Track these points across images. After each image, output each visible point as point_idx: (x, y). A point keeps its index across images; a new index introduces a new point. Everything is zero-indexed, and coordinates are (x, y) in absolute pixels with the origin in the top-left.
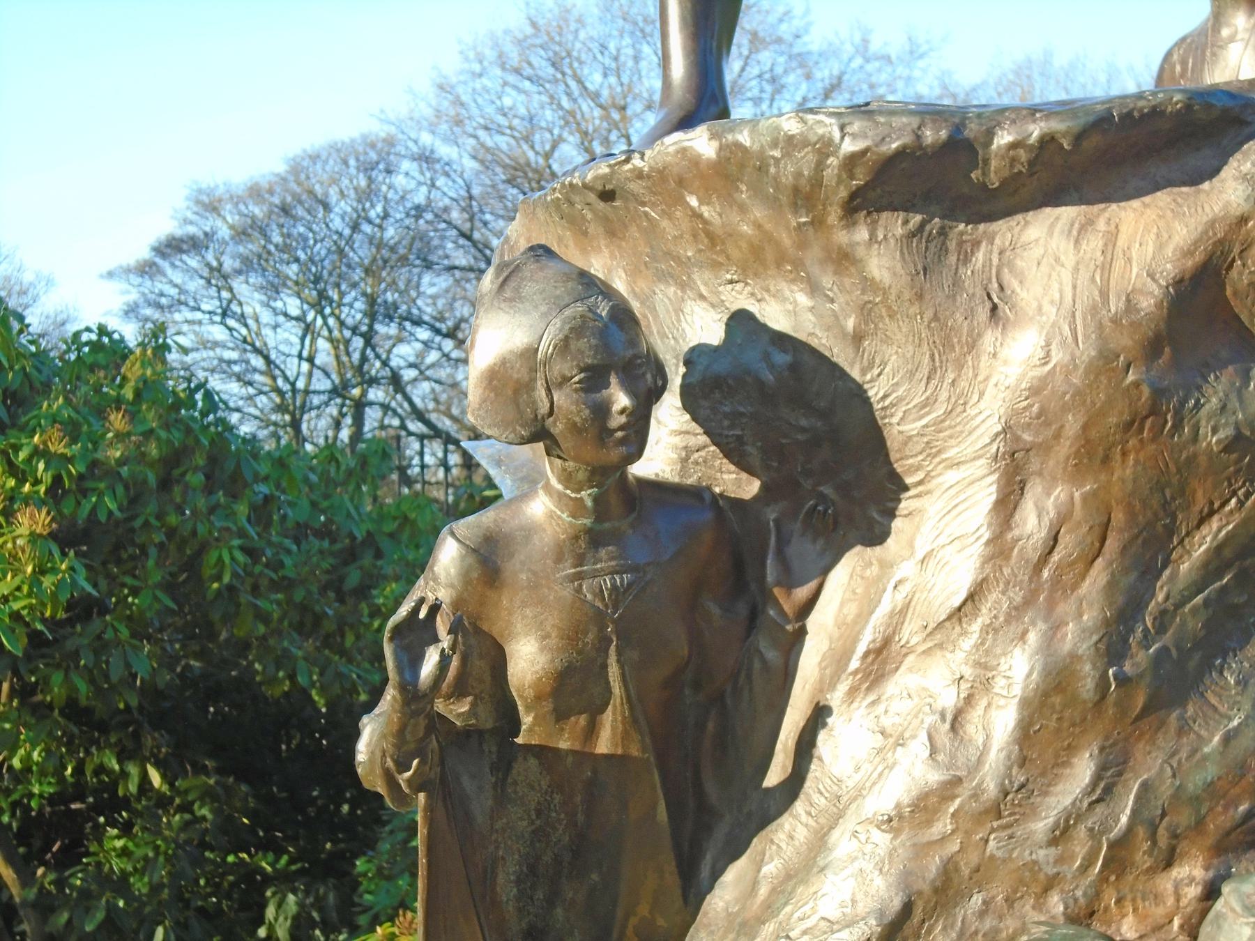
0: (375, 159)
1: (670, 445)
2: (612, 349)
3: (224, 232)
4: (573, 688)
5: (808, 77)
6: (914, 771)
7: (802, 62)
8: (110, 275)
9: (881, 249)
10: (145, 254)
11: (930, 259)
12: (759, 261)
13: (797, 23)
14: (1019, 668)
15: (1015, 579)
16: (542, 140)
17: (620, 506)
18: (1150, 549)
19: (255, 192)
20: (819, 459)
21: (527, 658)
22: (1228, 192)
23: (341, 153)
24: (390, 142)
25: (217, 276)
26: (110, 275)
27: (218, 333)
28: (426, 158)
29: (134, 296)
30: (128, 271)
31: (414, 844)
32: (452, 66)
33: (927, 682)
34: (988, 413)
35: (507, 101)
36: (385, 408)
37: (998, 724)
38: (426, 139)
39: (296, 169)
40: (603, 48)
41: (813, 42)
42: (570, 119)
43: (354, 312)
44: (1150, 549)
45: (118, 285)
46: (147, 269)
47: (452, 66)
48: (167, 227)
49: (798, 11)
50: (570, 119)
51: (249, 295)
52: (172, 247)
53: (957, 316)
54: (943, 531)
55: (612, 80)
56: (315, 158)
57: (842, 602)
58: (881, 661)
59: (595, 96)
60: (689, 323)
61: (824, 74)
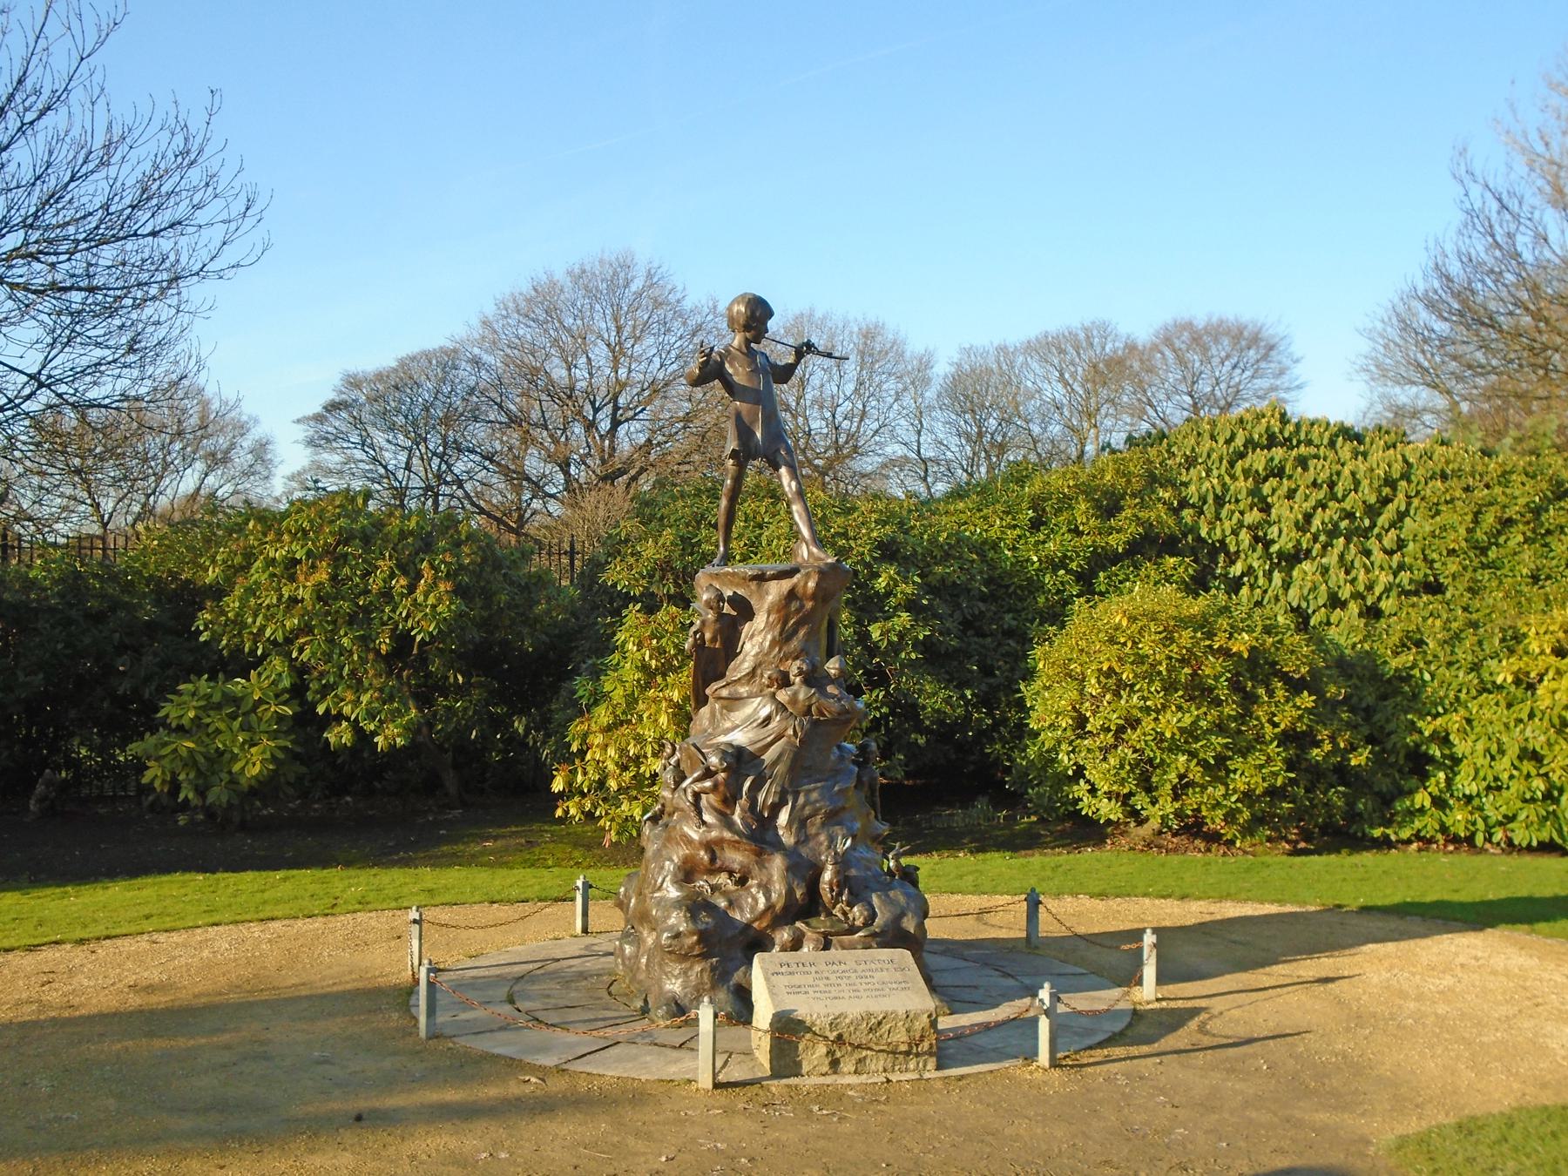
0: (447, 361)
1: (727, 609)
2: (720, 598)
3: (363, 399)
4: (714, 640)
5: (684, 324)
6: (756, 649)
7: (679, 314)
8: (298, 421)
9: (753, 585)
10: (319, 409)
11: (759, 586)
12: (737, 585)
13: (679, 296)
14: (769, 637)
15: (769, 626)
16: (540, 354)
17: (721, 616)
18: (785, 623)
19: (380, 377)
20: (745, 611)
21: (708, 636)
22: (795, 580)
23: (427, 356)
24: (455, 351)
25: (357, 422)
26: (298, 421)
27: (359, 454)
28: (476, 362)
29: (311, 432)
30: (309, 419)
31: (182, 796)
32: (490, 310)
33: (759, 639)
34: (766, 606)
35: (521, 332)
36: (452, 496)
37: (767, 644)
38: (476, 351)
39: (403, 363)
40: (574, 304)
41: (687, 304)
42: (555, 342)
43: (434, 442)
44: (785, 623)
45: (302, 427)
46: (319, 419)
47: (490, 310)
48: (331, 396)
49: (680, 288)
50: (555, 342)
51: (379, 438)
52: (333, 407)
53: (762, 595)
54: (760, 620)
55: (579, 322)
56: (413, 359)
57: (747, 628)
58: (753, 636)
59: (569, 330)
60: (728, 593)
61: (692, 323)
